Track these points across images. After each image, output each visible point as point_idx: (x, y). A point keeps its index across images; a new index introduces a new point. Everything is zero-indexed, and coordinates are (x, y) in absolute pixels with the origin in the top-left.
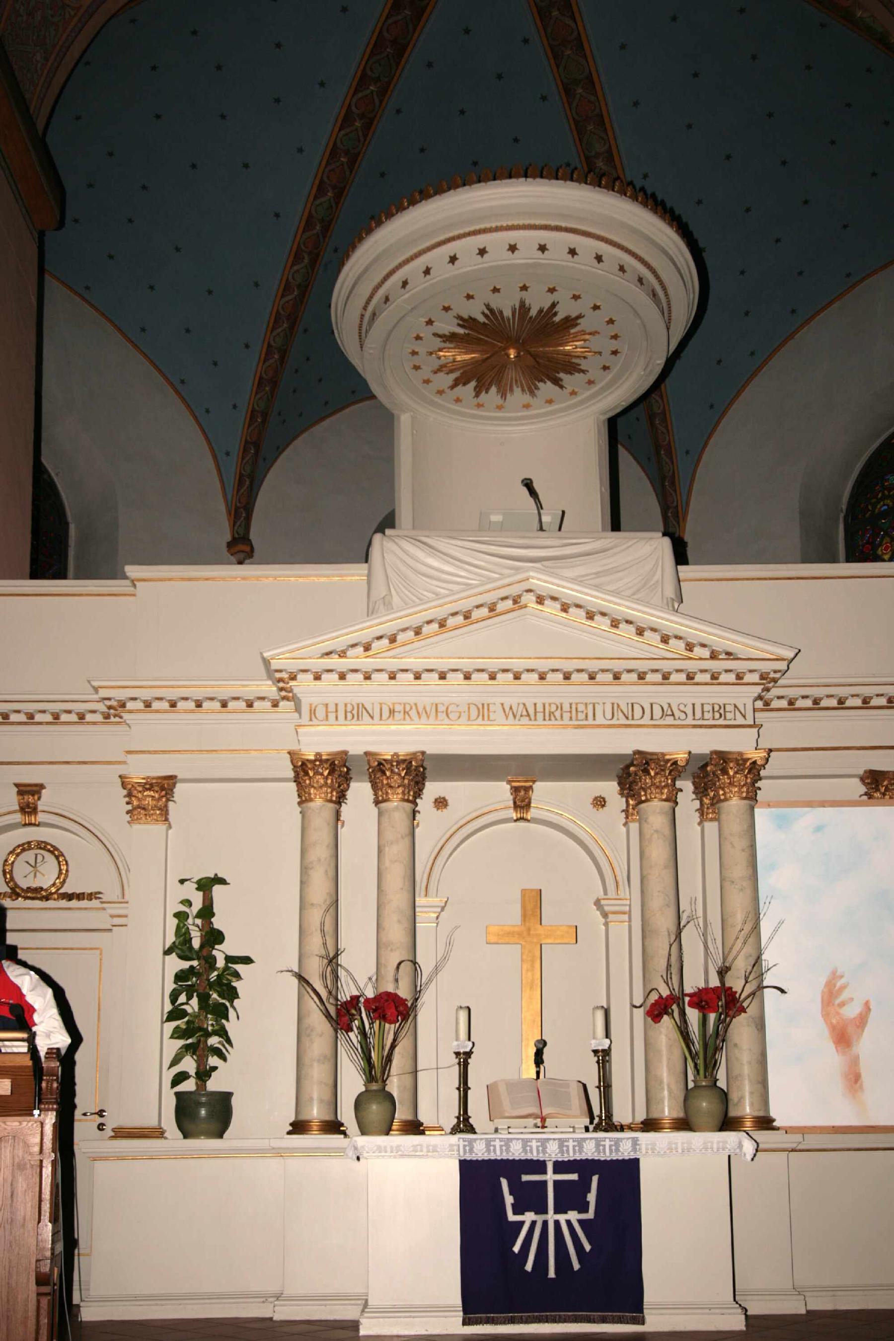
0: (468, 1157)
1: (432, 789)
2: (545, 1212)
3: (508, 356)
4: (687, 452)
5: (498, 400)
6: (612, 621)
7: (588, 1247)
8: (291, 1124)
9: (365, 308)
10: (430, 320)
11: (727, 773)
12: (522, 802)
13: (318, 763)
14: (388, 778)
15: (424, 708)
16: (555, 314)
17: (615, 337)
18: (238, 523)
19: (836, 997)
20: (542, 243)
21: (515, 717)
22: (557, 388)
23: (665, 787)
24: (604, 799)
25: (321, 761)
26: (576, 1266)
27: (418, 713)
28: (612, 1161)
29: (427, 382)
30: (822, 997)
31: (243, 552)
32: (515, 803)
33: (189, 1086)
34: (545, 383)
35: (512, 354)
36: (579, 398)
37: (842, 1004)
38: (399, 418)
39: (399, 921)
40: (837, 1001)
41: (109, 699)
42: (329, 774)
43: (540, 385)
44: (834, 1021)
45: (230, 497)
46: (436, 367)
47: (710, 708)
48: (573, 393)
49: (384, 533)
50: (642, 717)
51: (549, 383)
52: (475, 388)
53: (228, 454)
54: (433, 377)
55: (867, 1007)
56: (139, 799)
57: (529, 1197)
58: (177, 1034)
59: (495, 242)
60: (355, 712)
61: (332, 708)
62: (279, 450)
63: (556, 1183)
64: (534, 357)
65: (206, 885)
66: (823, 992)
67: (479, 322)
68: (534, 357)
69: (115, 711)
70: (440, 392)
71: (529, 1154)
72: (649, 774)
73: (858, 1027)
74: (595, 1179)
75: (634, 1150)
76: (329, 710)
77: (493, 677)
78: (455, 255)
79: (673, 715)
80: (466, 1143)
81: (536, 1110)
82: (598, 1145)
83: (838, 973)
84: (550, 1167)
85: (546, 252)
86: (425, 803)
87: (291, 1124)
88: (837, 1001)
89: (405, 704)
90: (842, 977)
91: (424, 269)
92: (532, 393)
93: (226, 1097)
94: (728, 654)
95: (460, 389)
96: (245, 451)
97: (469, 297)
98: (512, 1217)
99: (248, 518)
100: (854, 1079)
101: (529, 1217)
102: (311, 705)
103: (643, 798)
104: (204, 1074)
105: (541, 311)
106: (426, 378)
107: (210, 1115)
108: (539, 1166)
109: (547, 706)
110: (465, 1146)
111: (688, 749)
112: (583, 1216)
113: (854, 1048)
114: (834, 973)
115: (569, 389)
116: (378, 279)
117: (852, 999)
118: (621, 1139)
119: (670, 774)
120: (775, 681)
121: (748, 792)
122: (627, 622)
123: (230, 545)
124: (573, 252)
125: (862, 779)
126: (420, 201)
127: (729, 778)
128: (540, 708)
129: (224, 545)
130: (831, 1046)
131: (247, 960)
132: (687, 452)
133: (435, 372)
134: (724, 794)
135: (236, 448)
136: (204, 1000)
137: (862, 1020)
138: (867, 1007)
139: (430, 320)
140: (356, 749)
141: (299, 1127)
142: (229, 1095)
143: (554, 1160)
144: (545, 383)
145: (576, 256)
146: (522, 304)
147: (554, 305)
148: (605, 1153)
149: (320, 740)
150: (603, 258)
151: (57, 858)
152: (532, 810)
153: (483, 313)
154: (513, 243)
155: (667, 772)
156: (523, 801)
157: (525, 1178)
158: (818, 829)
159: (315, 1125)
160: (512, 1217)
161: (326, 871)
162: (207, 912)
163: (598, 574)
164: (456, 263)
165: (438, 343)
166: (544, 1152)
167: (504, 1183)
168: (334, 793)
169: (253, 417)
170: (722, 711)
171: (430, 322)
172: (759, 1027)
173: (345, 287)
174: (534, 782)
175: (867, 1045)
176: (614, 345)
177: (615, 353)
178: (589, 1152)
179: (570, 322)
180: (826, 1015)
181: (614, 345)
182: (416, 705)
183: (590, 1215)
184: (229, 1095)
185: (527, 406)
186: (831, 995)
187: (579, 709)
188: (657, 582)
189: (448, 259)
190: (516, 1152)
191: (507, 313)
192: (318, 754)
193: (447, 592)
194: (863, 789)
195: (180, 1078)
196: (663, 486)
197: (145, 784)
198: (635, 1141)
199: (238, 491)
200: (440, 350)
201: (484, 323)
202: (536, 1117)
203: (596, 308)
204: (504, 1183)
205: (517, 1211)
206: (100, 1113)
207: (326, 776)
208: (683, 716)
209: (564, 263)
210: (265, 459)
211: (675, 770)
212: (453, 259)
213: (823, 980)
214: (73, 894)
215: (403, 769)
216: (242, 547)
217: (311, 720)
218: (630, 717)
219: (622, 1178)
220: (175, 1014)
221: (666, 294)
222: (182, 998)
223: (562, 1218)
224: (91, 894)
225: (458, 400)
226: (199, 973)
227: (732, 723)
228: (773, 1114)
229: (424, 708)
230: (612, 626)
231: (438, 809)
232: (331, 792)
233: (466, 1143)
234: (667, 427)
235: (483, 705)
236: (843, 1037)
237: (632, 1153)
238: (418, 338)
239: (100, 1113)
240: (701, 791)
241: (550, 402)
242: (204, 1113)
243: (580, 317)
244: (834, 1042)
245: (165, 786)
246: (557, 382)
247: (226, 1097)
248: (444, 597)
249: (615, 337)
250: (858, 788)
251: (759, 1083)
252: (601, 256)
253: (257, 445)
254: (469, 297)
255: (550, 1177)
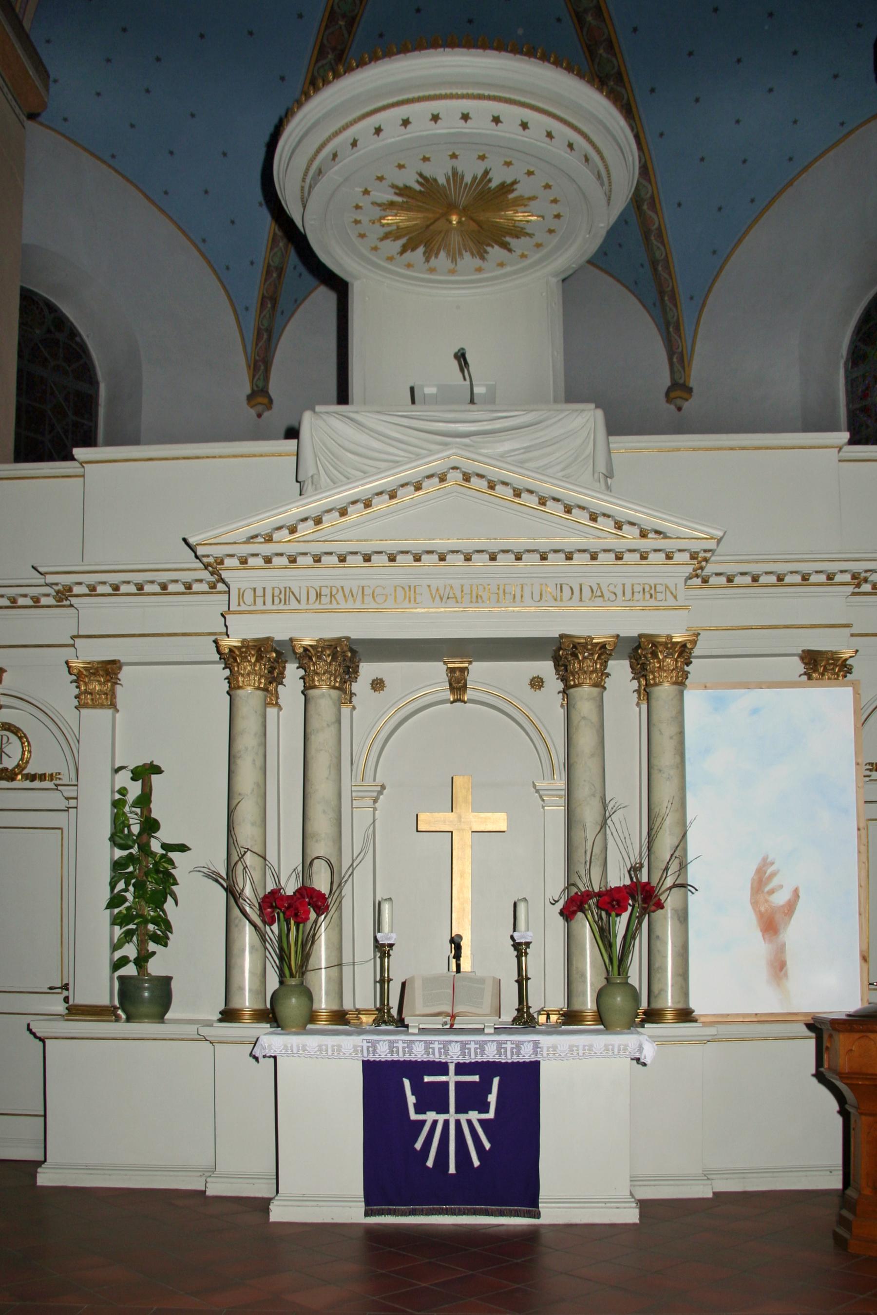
0: (371, 1058)
1: (368, 670)
2: (447, 1111)
3: (450, 222)
4: (691, 298)
5: (449, 265)
6: (540, 499)
7: (487, 1146)
8: (220, 1013)
9: (304, 180)
10: (366, 189)
11: (656, 657)
12: (458, 685)
13: (244, 650)
14: (314, 664)
15: (351, 591)
16: (490, 181)
17: (555, 201)
18: (257, 377)
19: (766, 884)
20: (465, 112)
21: (441, 599)
22: (505, 252)
23: (592, 672)
24: (542, 679)
25: (248, 647)
26: (476, 1163)
27: (345, 596)
28: (513, 1063)
29: (375, 249)
30: (752, 885)
31: (260, 404)
32: (450, 684)
33: (130, 970)
34: (493, 247)
35: (454, 219)
36: (508, 269)
37: (772, 892)
38: (353, 285)
39: (324, 812)
40: (767, 889)
41: (57, 584)
42: (257, 660)
43: (489, 249)
44: (763, 909)
45: (249, 350)
46: (381, 235)
47: (640, 588)
48: (523, 256)
49: (314, 410)
50: (571, 598)
51: (496, 247)
52: (424, 253)
53: (247, 309)
54: (381, 245)
55: (796, 894)
56: (86, 684)
57: (433, 1098)
58: (116, 921)
59: (419, 111)
60: (282, 596)
61: (259, 592)
62: (297, 304)
63: (457, 1084)
64: (479, 224)
65: (145, 773)
66: (753, 879)
67: (415, 191)
68: (479, 224)
69: (64, 595)
70: (390, 259)
71: (431, 1056)
72: (577, 657)
73: (786, 915)
74: (496, 1081)
75: (535, 1053)
76: (257, 594)
77: (417, 559)
78: (408, 119)
79: (602, 596)
80: (370, 1044)
81: (448, 1009)
82: (499, 1049)
83: (769, 860)
84: (452, 1068)
85: (469, 121)
86: (361, 686)
87: (220, 1013)
88: (767, 889)
89: (331, 587)
90: (772, 864)
91: (352, 141)
92: (483, 258)
93: (165, 983)
94: (657, 532)
95: (408, 255)
96: (263, 305)
97: (401, 167)
98: (413, 1116)
99: (267, 371)
100: (779, 967)
101: (430, 1116)
102: (239, 589)
103: (572, 683)
104: (142, 960)
105: (475, 178)
106: (373, 245)
107: (151, 999)
108: (441, 1068)
109: (474, 587)
110: (368, 1047)
111: (614, 633)
112: (484, 1116)
113: (781, 936)
114: (765, 859)
115: (519, 252)
116: (312, 152)
117: (781, 887)
118: (522, 1042)
119: (599, 658)
120: (706, 560)
121: (677, 677)
122: (555, 499)
123: (250, 398)
124: (496, 120)
125: (802, 658)
126: (370, 62)
127: (659, 662)
128: (467, 590)
129: (245, 398)
130: (759, 934)
131: (182, 848)
132: (691, 298)
133: (382, 239)
134: (654, 679)
135: (254, 302)
136: (140, 887)
137: (790, 908)
138: (796, 894)
139: (366, 189)
140: (280, 635)
141: (229, 1015)
142: (168, 979)
143: (456, 1061)
144: (493, 247)
145: (500, 124)
146: (455, 173)
147: (486, 173)
148: (506, 1056)
149: (243, 630)
150: (529, 125)
151: (20, 738)
152: (468, 691)
153: (418, 182)
154: (435, 113)
155: (596, 656)
156: (459, 683)
157: (427, 1079)
158: (755, 711)
159: (247, 1013)
160: (413, 1116)
161: (254, 760)
162: (144, 800)
163: (528, 449)
164: (381, 134)
165: (377, 212)
166: (446, 1053)
167: (407, 1083)
168: (263, 681)
169: (268, 273)
170: (652, 592)
171: (366, 192)
172: (682, 919)
173: (283, 159)
174: (470, 663)
175: (793, 934)
176: (555, 209)
177: (558, 216)
178: (491, 1054)
179: (506, 188)
180: (755, 903)
181: (555, 209)
182: (342, 587)
183: (491, 1115)
184: (168, 979)
185: (479, 270)
186: (761, 882)
187: (507, 591)
188: (589, 456)
189: (374, 131)
190: (419, 1054)
191: (442, 180)
192: (243, 641)
193: (374, 470)
194: (801, 668)
195: (118, 964)
196: (668, 333)
197: (91, 668)
198: (536, 1044)
199: (257, 345)
200: (383, 218)
201: (420, 192)
202: (447, 1015)
203: (530, 173)
204: (407, 1083)
205: (419, 1110)
206: (66, 987)
207: (261, 662)
208: (613, 597)
209: (488, 132)
210: (282, 313)
211: (603, 652)
212: (378, 131)
213: (753, 868)
214: (35, 775)
215: (329, 655)
216: (260, 400)
217: (239, 605)
218: (559, 598)
219: (523, 1080)
220: (115, 901)
221: (602, 158)
222: (121, 885)
223: (463, 1118)
224: (52, 774)
225: (409, 266)
226: (138, 859)
227: (663, 603)
228: (692, 1005)
229: (351, 591)
230: (539, 503)
231: (383, 690)
232: (259, 679)
233: (370, 1044)
234: (670, 274)
235: (410, 587)
236: (771, 925)
237: (533, 1056)
238: (357, 207)
239: (66, 987)
240: (640, 670)
241: (501, 265)
242: (143, 998)
243: (515, 182)
244: (761, 931)
245: (109, 670)
246: (505, 246)
247: (165, 983)
248: (373, 475)
249: (555, 201)
250: (799, 667)
251: (680, 975)
252: (527, 123)
253: (274, 300)
254: (401, 167)
255: (452, 1079)
